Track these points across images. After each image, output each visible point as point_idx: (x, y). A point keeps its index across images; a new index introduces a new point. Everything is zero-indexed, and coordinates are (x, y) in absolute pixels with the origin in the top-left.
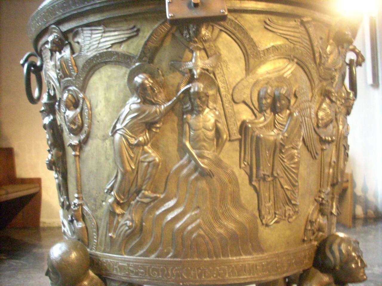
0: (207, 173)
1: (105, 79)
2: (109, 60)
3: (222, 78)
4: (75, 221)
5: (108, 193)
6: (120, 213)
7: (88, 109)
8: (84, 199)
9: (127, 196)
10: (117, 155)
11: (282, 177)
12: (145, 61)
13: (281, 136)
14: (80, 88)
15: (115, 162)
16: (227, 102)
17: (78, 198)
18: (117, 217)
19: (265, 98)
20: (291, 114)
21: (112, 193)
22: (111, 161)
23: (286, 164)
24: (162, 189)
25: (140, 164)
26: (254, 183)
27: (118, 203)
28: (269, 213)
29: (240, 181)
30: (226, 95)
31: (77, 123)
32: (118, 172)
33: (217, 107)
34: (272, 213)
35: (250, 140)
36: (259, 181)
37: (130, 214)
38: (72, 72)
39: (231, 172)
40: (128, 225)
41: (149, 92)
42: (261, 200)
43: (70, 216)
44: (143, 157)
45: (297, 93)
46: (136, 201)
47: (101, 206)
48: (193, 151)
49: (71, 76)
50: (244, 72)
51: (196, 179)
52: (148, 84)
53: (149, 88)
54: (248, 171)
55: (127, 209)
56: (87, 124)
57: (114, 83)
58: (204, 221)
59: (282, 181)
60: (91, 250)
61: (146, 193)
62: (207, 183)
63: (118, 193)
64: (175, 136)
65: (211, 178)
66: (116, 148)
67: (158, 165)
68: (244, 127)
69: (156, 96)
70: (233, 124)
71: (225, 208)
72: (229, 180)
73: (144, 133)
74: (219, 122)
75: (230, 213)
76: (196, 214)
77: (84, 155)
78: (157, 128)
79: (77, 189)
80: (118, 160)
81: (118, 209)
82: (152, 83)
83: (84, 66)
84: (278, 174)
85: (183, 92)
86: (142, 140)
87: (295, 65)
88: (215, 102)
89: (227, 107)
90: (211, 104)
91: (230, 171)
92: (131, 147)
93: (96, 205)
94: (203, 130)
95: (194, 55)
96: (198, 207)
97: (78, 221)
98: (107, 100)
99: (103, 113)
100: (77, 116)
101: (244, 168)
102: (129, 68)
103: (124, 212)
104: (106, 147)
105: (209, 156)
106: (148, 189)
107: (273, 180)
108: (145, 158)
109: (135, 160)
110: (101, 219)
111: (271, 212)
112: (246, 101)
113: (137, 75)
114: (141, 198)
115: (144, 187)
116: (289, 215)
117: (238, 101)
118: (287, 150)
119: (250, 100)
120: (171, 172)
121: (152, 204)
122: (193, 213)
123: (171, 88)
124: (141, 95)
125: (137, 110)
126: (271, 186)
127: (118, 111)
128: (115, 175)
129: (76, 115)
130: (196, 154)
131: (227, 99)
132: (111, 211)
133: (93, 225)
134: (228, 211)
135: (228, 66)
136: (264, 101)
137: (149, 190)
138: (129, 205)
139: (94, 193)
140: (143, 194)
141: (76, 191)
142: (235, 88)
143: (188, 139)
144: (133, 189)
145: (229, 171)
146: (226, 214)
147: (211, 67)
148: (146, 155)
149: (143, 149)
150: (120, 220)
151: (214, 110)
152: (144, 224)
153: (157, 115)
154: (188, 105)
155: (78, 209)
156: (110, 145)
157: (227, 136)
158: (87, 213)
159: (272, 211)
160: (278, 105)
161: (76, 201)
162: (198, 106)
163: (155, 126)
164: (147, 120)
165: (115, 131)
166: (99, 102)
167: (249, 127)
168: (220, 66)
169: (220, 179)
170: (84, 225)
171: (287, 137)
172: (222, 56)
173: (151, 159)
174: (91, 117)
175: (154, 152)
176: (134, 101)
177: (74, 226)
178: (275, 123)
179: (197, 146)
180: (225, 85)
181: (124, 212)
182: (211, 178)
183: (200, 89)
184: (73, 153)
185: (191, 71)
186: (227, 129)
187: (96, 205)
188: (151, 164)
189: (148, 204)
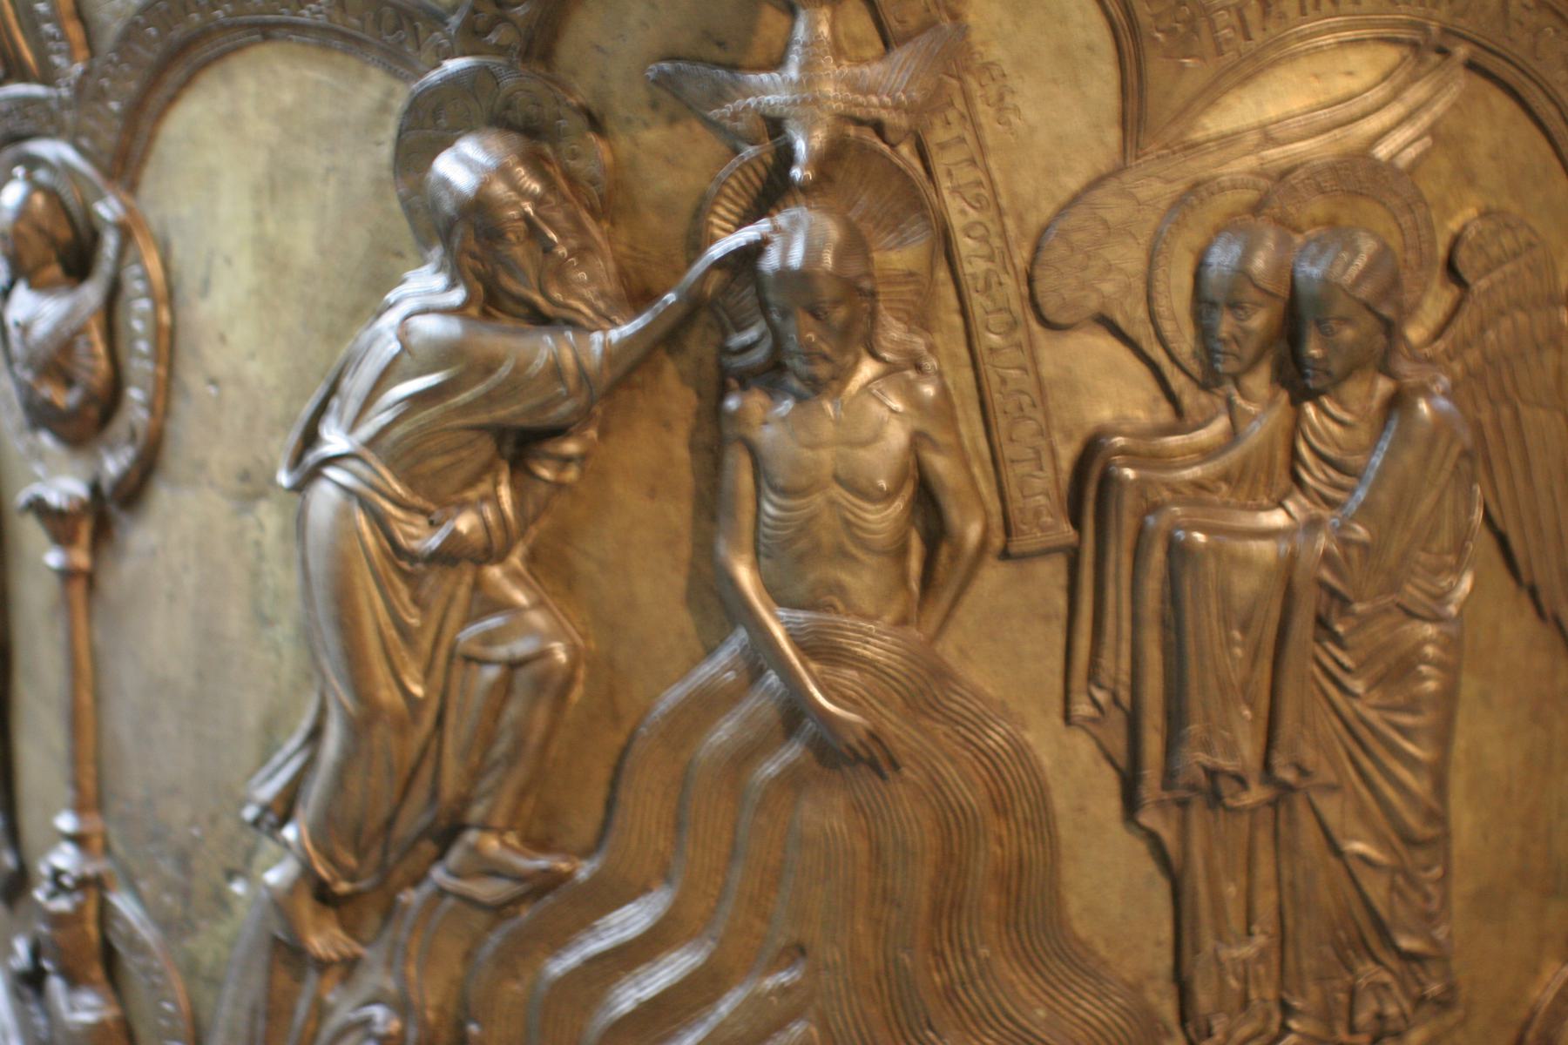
0: (849, 747)
1: (261, 128)
2: (286, 16)
3: (966, 175)
4: (56, 985)
5: (265, 826)
6: (334, 956)
7: (150, 293)
8: (118, 848)
9: (375, 854)
10: (323, 611)
11: (1332, 788)
12: (500, 50)
13: (1322, 542)
14: (106, 160)
15: (307, 636)
16: (993, 320)
17: (78, 840)
18: (312, 977)
19: (1234, 306)
20: (1398, 402)
21: (290, 833)
22: (284, 631)
23: (1358, 705)
24: (585, 825)
25: (458, 672)
26: (1149, 818)
27: (323, 895)
28: (1245, 1003)
29: (1060, 802)
30: (994, 280)
31: (82, 375)
32: (322, 711)
33: (931, 348)
34: (1264, 1000)
35: (1126, 560)
36: (1183, 804)
37: (389, 964)
38: (59, 52)
39: (1007, 747)
40: (380, 1029)
41: (519, 252)
42: (1195, 919)
43: (21, 947)
44: (474, 630)
45: (1463, 255)
46: (426, 889)
47: (222, 902)
48: (777, 618)
49: (47, 76)
50: (1113, 136)
51: (792, 780)
52: (515, 205)
53: (517, 229)
54: (1119, 745)
55: (379, 934)
56: (143, 387)
57: (313, 159)
58: (829, 1029)
59: (1331, 808)
60: (894, 119)
61: (492, 844)
62: (857, 807)
63: (322, 833)
64: (678, 513)
65: (879, 782)
66: (317, 565)
67: (569, 681)
68: (1095, 472)
69: (560, 272)
70: (1030, 454)
71: (965, 961)
72: (990, 791)
73: (484, 487)
74: (936, 447)
75: (990, 991)
76: (784, 990)
77: (123, 574)
78: (566, 460)
79: (76, 785)
80: (330, 639)
81: (319, 930)
82: (538, 201)
83: (131, 33)
84: (1302, 771)
85: (720, 264)
86: (472, 530)
87: (1459, 83)
88: (921, 320)
89: (992, 350)
90: (894, 331)
91: (1002, 742)
92: (405, 565)
93: (186, 894)
94: (837, 492)
95: (801, 32)
96: (797, 951)
97: (74, 980)
98: (272, 259)
99: (242, 335)
100: (82, 330)
101: (1093, 720)
102: (406, 80)
103: (359, 950)
104: (258, 544)
105: (869, 652)
106: (499, 821)
107: (1273, 804)
108: (489, 639)
109: (426, 643)
110: (215, 982)
111: (1253, 994)
112: (1120, 319)
113: (445, 143)
114: (455, 874)
115: (477, 812)
116: (1380, 1017)
117: (1063, 319)
118: (1364, 621)
119: (1141, 312)
120: (643, 730)
121: (526, 913)
122: (769, 983)
123: (653, 221)
124: (468, 261)
125: (444, 354)
126: (1263, 837)
127: (334, 336)
128: (305, 724)
129: (74, 324)
130: (792, 636)
131: (994, 300)
132: (276, 942)
133: (168, 1016)
134: (980, 982)
135: (1008, 99)
136: (1225, 325)
137: (510, 828)
138: (390, 911)
139: (178, 813)
140: (474, 850)
141: (67, 794)
142: (1044, 230)
143: (747, 537)
144: (414, 818)
145: (995, 738)
146: (969, 997)
147: (897, 106)
148: (493, 622)
149: (478, 585)
150: (330, 998)
151: (911, 374)
152: (473, 1028)
153: (561, 389)
154: (750, 335)
155: (79, 909)
156: (283, 535)
157: (986, 530)
158: (132, 939)
159: (1265, 992)
160: (1314, 351)
161: (65, 858)
162: (811, 355)
163: (549, 447)
164: (501, 413)
165: (311, 458)
166: (219, 262)
167: (1122, 482)
168: (959, 102)
169: (939, 787)
170: (110, 1013)
171: (1364, 547)
172: (975, 37)
173: (521, 647)
174: (168, 344)
175: (549, 601)
176: (431, 293)
177: (49, 1013)
178: (1294, 455)
179: (800, 590)
180: (987, 217)
181: (359, 950)
182: (883, 777)
183: (820, 260)
184: (54, 558)
185: (775, 126)
186: (994, 488)
187: (186, 894)
188: (523, 675)
189: (499, 910)
